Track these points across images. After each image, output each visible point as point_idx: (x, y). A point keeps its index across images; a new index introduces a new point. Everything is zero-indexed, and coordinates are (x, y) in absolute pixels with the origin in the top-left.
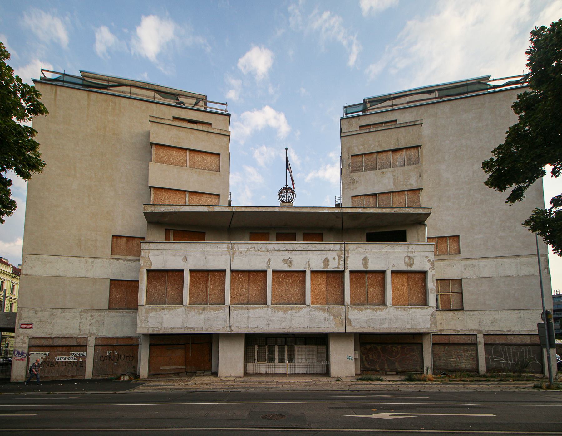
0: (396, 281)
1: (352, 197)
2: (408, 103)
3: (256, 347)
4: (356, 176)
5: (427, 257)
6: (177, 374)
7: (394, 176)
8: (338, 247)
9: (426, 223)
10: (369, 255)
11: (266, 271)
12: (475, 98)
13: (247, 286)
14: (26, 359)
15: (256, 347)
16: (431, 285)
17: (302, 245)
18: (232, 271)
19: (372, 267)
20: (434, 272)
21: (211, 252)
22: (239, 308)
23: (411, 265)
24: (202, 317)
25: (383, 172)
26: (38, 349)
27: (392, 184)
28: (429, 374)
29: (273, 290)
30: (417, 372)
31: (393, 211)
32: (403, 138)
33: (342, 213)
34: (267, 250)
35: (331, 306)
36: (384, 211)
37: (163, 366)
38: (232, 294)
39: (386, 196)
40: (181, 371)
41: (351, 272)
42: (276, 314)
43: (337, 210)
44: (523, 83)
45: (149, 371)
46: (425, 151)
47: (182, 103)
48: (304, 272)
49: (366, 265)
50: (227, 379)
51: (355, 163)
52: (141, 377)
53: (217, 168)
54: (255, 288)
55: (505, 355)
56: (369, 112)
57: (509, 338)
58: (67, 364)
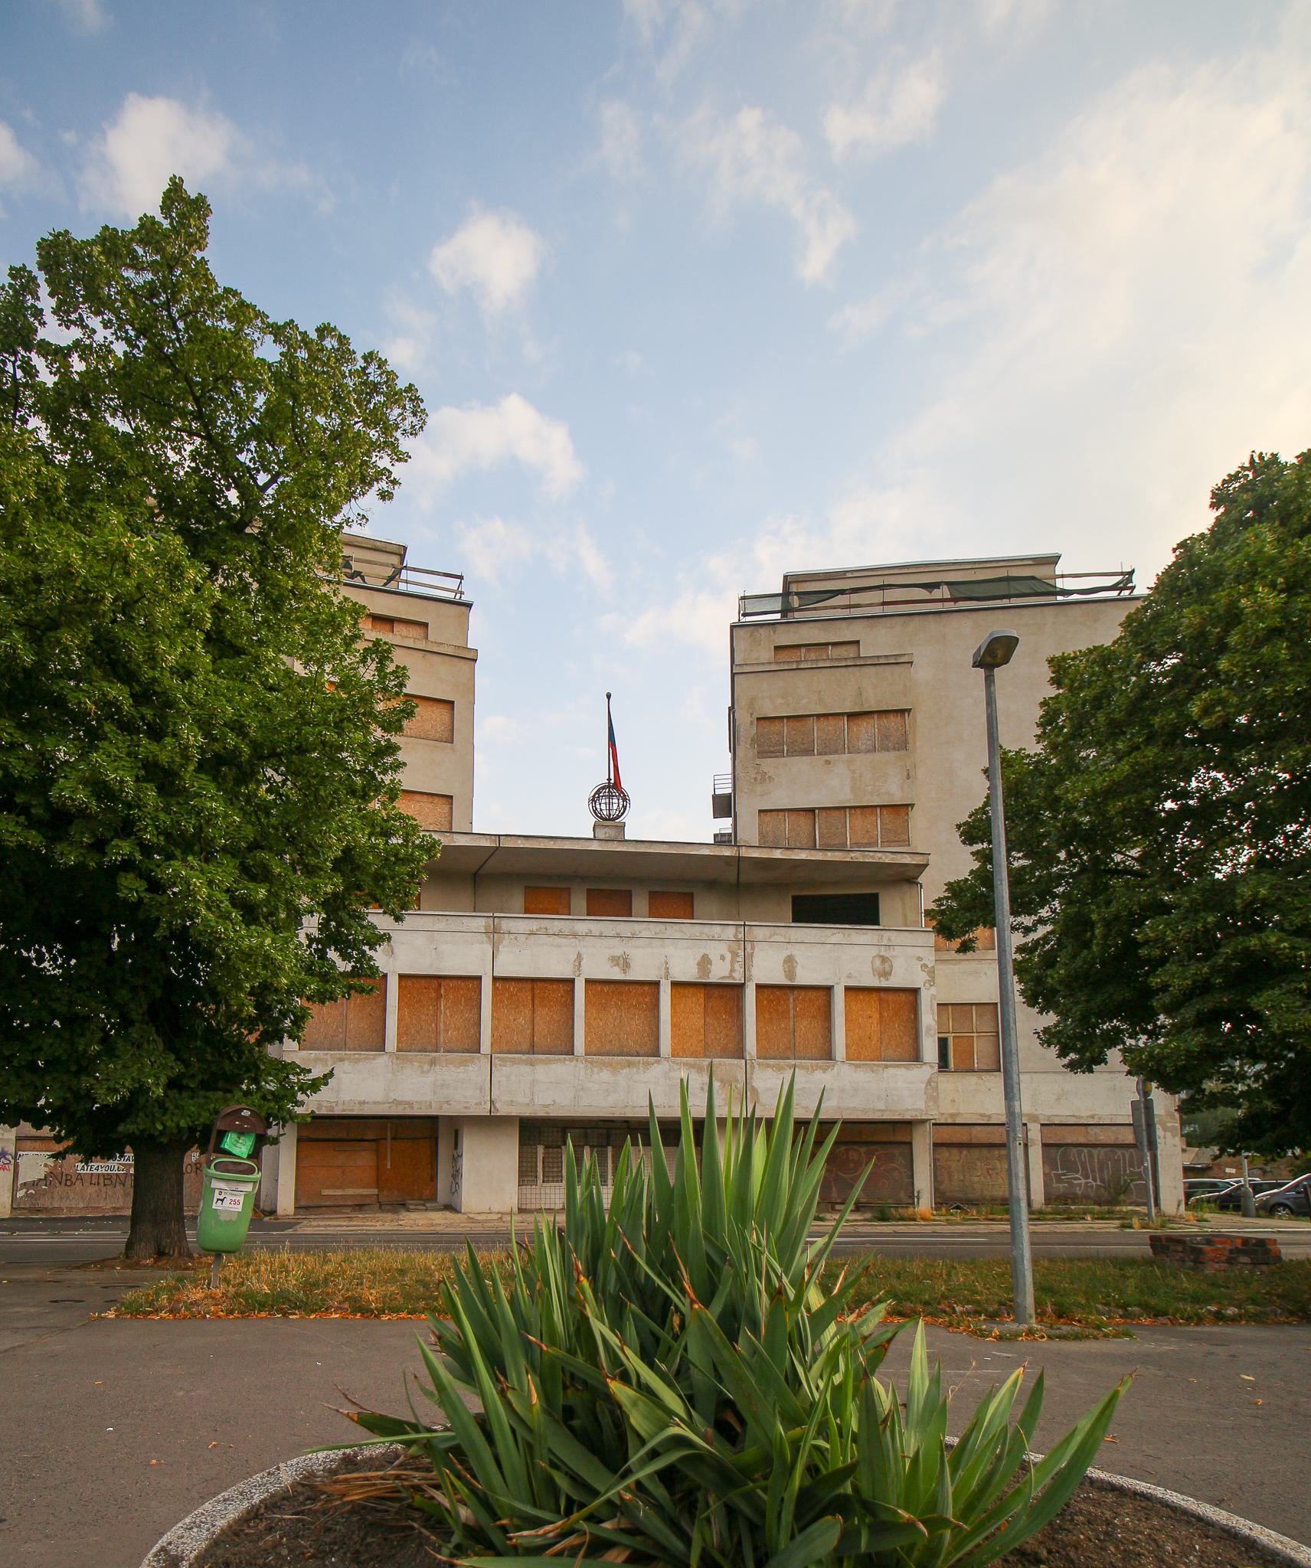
1: (760, 811)
2: (884, 604)
3: (540, 1150)
4: (768, 764)
5: (919, 959)
6: (360, 1207)
7: (853, 772)
8: (730, 932)
9: (920, 880)
10: (797, 952)
11: (572, 981)
12: (1025, 611)
13: (529, 1014)
14: (12, 1167)
16: (928, 1018)
18: (495, 979)
19: (803, 978)
20: (933, 991)
22: (514, 1062)
23: (886, 974)
24: (430, 1079)
25: (828, 762)
26: (38, 1144)
28: (925, 1203)
29: (588, 1024)
30: (899, 1204)
31: (848, 857)
33: (739, 859)
34: (575, 935)
35: (716, 1061)
36: (830, 856)
37: (328, 1188)
38: (494, 1029)
40: (368, 1201)
41: (759, 987)
42: (595, 1076)
43: (727, 852)
44: (1121, 589)
46: (922, 723)
47: (358, 574)
48: (657, 984)
49: (790, 972)
51: (762, 735)
52: (280, 1211)
53: (446, 735)
54: (546, 1019)
55: (1084, 1168)
56: (797, 616)
58: (101, 1180)
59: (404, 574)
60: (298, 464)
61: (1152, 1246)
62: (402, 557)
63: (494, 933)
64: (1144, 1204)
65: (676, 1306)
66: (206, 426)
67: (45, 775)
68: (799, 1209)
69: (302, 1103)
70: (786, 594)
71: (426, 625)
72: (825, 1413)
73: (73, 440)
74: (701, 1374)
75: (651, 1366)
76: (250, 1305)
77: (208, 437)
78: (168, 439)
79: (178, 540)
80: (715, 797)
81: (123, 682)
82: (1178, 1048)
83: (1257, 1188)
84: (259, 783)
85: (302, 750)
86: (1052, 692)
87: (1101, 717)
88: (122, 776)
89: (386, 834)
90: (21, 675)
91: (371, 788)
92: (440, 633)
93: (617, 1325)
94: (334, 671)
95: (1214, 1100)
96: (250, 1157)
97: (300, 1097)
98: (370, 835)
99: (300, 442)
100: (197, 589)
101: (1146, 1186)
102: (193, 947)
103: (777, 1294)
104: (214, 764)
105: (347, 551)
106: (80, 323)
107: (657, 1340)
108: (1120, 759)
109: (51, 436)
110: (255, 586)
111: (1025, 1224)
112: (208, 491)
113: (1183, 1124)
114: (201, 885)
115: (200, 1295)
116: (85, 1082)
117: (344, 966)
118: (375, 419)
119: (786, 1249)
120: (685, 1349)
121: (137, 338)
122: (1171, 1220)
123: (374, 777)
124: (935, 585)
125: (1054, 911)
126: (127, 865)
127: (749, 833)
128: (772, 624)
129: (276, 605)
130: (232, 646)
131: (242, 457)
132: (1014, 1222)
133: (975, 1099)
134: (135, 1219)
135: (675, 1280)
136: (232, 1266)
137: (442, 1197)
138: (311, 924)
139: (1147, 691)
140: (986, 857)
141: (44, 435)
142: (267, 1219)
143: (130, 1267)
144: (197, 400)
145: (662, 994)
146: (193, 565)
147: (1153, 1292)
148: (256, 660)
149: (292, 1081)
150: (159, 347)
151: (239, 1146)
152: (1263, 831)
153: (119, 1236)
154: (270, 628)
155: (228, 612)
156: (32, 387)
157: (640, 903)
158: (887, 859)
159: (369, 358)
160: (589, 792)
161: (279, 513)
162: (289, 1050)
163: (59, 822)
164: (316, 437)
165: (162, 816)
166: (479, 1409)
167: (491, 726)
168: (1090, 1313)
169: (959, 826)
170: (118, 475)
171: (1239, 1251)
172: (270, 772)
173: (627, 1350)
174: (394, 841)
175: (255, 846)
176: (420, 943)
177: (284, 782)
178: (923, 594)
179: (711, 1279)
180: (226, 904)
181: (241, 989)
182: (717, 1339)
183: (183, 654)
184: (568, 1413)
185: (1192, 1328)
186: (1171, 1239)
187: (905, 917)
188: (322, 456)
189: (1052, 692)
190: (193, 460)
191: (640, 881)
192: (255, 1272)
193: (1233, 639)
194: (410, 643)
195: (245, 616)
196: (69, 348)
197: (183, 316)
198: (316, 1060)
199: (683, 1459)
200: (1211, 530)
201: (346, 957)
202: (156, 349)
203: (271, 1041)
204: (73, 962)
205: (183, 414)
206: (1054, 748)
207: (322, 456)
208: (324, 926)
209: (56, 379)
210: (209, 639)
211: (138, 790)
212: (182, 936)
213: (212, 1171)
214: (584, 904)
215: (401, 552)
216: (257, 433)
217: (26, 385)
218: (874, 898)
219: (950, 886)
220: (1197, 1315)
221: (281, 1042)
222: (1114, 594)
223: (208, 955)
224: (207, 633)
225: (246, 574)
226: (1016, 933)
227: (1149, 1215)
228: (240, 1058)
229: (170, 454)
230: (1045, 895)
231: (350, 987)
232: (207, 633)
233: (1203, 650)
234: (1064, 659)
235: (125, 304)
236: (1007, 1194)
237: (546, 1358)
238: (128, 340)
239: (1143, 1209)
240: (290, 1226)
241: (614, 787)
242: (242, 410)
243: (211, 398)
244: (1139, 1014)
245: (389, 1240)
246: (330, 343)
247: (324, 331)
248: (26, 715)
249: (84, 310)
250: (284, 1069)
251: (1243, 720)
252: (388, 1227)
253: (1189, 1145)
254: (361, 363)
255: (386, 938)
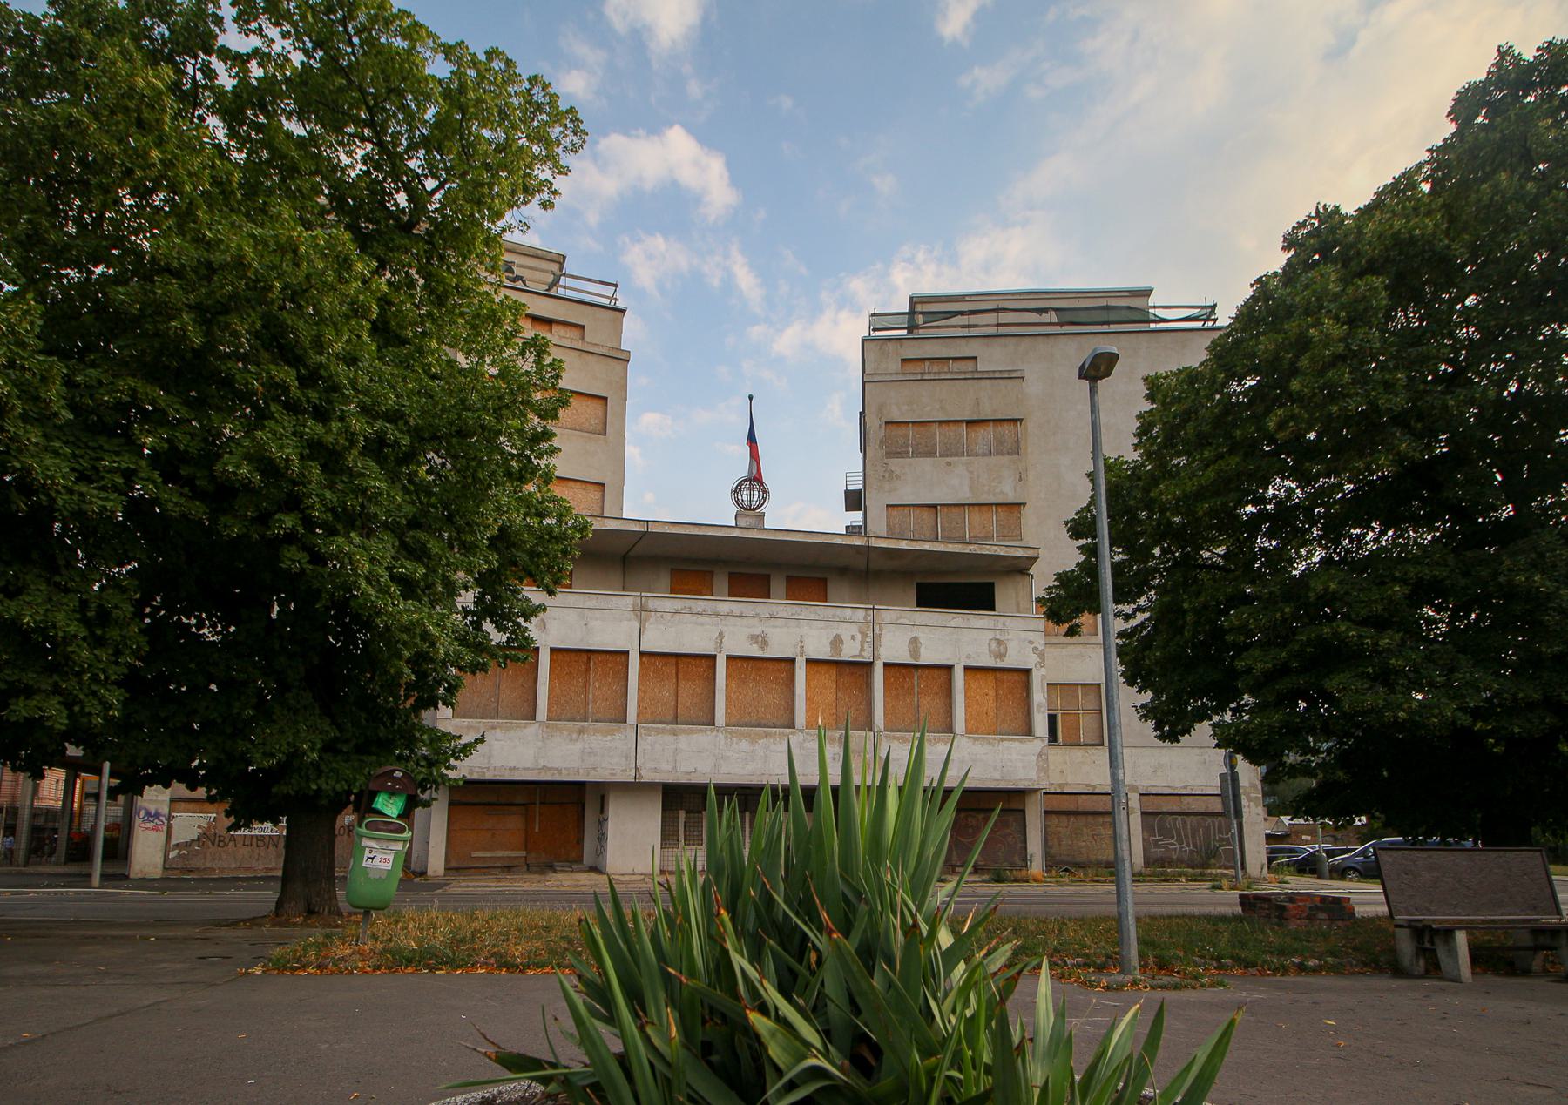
0: (974, 685)
2: (999, 325)
3: (682, 814)
4: (895, 464)
5: (1031, 642)
6: (508, 868)
8: (860, 615)
10: (922, 634)
11: (714, 657)
12: (1123, 337)
13: (672, 687)
15: (682, 814)
16: (1039, 696)
17: (789, 608)
18: (642, 654)
19: (926, 658)
20: (1043, 671)
21: (598, 613)
22: (658, 732)
23: (1001, 656)
24: (577, 747)
25: (949, 464)
26: (191, 806)
27: (966, 489)
28: (1037, 867)
29: (728, 697)
30: (1013, 866)
32: (990, 401)
36: (951, 548)
39: (955, 510)
41: (886, 665)
43: (857, 542)
44: (1205, 321)
45: (447, 860)
46: (1031, 427)
47: (520, 278)
48: (793, 661)
49: (915, 652)
50: (627, 878)
51: (888, 438)
52: (430, 873)
53: (599, 427)
54: (689, 691)
55: (1179, 835)
56: (922, 333)
57: (1186, 800)
59: (563, 280)
60: (465, 173)
61: (1242, 904)
62: (561, 265)
63: (641, 611)
64: (1234, 867)
65: (814, 945)
66: (377, 133)
67: (212, 449)
68: (931, 850)
69: (455, 768)
70: (912, 312)
71: (582, 327)
72: (960, 1042)
73: (248, 138)
74: (837, 1010)
75: (790, 1000)
76: (398, 960)
77: (380, 144)
78: (340, 143)
79: (347, 236)
80: (847, 492)
81: (290, 365)
82: (1261, 725)
83: (1331, 854)
84: (419, 464)
85: (463, 434)
86: (1147, 406)
87: (1190, 427)
88: (286, 452)
89: (541, 515)
90: (189, 355)
91: (527, 472)
92: (596, 335)
93: (756, 958)
94: (493, 364)
95: (1294, 771)
96: (399, 817)
97: (452, 761)
98: (526, 515)
99: (467, 152)
100: (364, 282)
101: (1233, 851)
102: (351, 614)
103: (911, 930)
104: (376, 448)
105: (507, 257)
106: (260, 32)
107: (794, 975)
108: (1207, 466)
109: (227, 135)
110: (421, 282)
111: (1129, 883)
112: (379, 196)
113: (1265, 795)
114: (367, 560)
115: (348, 951)
116: (241, 746)
117: (497, 637)
118: (539, 136)
119: (919, 889)
120: (822, 984)
121: (314, 49)
122: (1256, 881)
123: (530, 461)
124: (1045, 310)
125: (1150, 600)
126: (291, 538)
127: (878, 525)
128: (899, 339)
129: (440, 301)
130: (397, 337)
131: (412, 164)
132: (1118, 884)
133: (1083, 770)
134: (286, 880)
135: (812, 917)
136: (380, 922)
137: (588, 859)
138: (467, 599)
139: (1229, 408)
140: (1091, 551)
141: (221, 135)
142: (417, 880)
143: (281, 925)
144: (370, 110)
145: (798, 671)
146: (360, 258)
147: (1243, 945)
148: (420, 350)
149: (445, 749)
150: (335, 59)
151: (390, 807)
152: (1333, 533)
153: (268, 897)
154: (434, 321)
155: (393, 304)
156: (211, 89)
157: (778, 585)
158: (1002, 552)
159: (533, 80)
160: (732, 484)
161: (445, 217)
162: (443, 718)
163: (224, 494)
164: (482, 148)
165: (328, 494)
166: (617, 1047)
167: (644, 425)
168: (1188, 964)
169: (1066, 523)
170: (291, 171)
171: (1317, 908)
172: (431, 455)
173: (766, 983)
174: (547, 521)
175: (414, 524)
176: (568, 618)
177: (443, 465)
178: (1034, 317)
179: (846, 915)
180: (385, 579)
181: (400, 657)
182: (855, 968)
183: (349, 342)
184: (707, 1049)
185: (1278, 978)
186: (1257, 897)
187: (1018, 605)
188: (487, 167)
189: (1147, 406)
190: (365, 163)
191: (778, 566)
192: (403, 929)
193: (1304, 362)
194: (567, 343)
195: (412, 306)
196: (248, 55)
197: (358, 32)
198: (469, 727)
199: (818, 1091)
200: (1284, 269)
201: (501, 629)
202: (331, 61)
203: (426, 707)
204: (232, 629)
205: (357, 121)
206: (1148, 455)
207: (487, 167)
208: (479, 601)
209: (235, 82)
210: (375, 329)
211: (303, 467)
212: (342, 606)
213: (363, 830)
214: (725, 588)
215: (560, 260)
216: (426, 142)
217: (205, 87)
218: (989, 589)
219: (1059, 577)
220: (1283, 966)
221: (436, 708)
222: (1199, 324)
223: (368, 625)
224: (373, 323)
225: (413, 271)
226: (1117, 619)
227: (1236, 877)
228: (393, 724)
229: (343, 157)
230: (1141, 587)
231: (506, 657)
232: (373, 323)
233: (1276, 373)
234: (1157, 377)
235: (303, 18)
236: (1112, 858)
237: (685, 992)
238: (306, 52)
239: (1231, 872)
240: (439, 886)
241: (755, 479)
242: (411, 119)
243: (384, 109)
244: (1224, 695)
245: (534, 898)
246: (497, 65)
247: (492, 54)
248: (193, 393)
249: (264, 20)
250: (437, 737)
251: (1312, 436)
252: (534, 887)
253: (1270, 814)
254: (526, 85)
255: (542, 608)
